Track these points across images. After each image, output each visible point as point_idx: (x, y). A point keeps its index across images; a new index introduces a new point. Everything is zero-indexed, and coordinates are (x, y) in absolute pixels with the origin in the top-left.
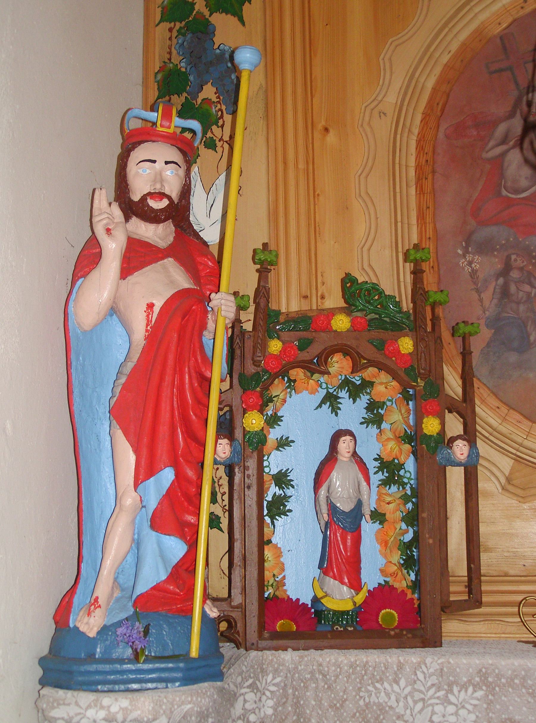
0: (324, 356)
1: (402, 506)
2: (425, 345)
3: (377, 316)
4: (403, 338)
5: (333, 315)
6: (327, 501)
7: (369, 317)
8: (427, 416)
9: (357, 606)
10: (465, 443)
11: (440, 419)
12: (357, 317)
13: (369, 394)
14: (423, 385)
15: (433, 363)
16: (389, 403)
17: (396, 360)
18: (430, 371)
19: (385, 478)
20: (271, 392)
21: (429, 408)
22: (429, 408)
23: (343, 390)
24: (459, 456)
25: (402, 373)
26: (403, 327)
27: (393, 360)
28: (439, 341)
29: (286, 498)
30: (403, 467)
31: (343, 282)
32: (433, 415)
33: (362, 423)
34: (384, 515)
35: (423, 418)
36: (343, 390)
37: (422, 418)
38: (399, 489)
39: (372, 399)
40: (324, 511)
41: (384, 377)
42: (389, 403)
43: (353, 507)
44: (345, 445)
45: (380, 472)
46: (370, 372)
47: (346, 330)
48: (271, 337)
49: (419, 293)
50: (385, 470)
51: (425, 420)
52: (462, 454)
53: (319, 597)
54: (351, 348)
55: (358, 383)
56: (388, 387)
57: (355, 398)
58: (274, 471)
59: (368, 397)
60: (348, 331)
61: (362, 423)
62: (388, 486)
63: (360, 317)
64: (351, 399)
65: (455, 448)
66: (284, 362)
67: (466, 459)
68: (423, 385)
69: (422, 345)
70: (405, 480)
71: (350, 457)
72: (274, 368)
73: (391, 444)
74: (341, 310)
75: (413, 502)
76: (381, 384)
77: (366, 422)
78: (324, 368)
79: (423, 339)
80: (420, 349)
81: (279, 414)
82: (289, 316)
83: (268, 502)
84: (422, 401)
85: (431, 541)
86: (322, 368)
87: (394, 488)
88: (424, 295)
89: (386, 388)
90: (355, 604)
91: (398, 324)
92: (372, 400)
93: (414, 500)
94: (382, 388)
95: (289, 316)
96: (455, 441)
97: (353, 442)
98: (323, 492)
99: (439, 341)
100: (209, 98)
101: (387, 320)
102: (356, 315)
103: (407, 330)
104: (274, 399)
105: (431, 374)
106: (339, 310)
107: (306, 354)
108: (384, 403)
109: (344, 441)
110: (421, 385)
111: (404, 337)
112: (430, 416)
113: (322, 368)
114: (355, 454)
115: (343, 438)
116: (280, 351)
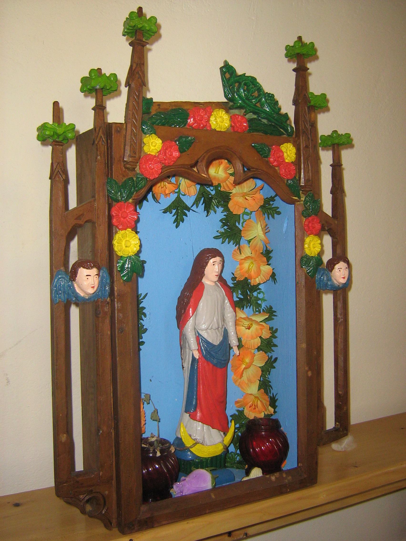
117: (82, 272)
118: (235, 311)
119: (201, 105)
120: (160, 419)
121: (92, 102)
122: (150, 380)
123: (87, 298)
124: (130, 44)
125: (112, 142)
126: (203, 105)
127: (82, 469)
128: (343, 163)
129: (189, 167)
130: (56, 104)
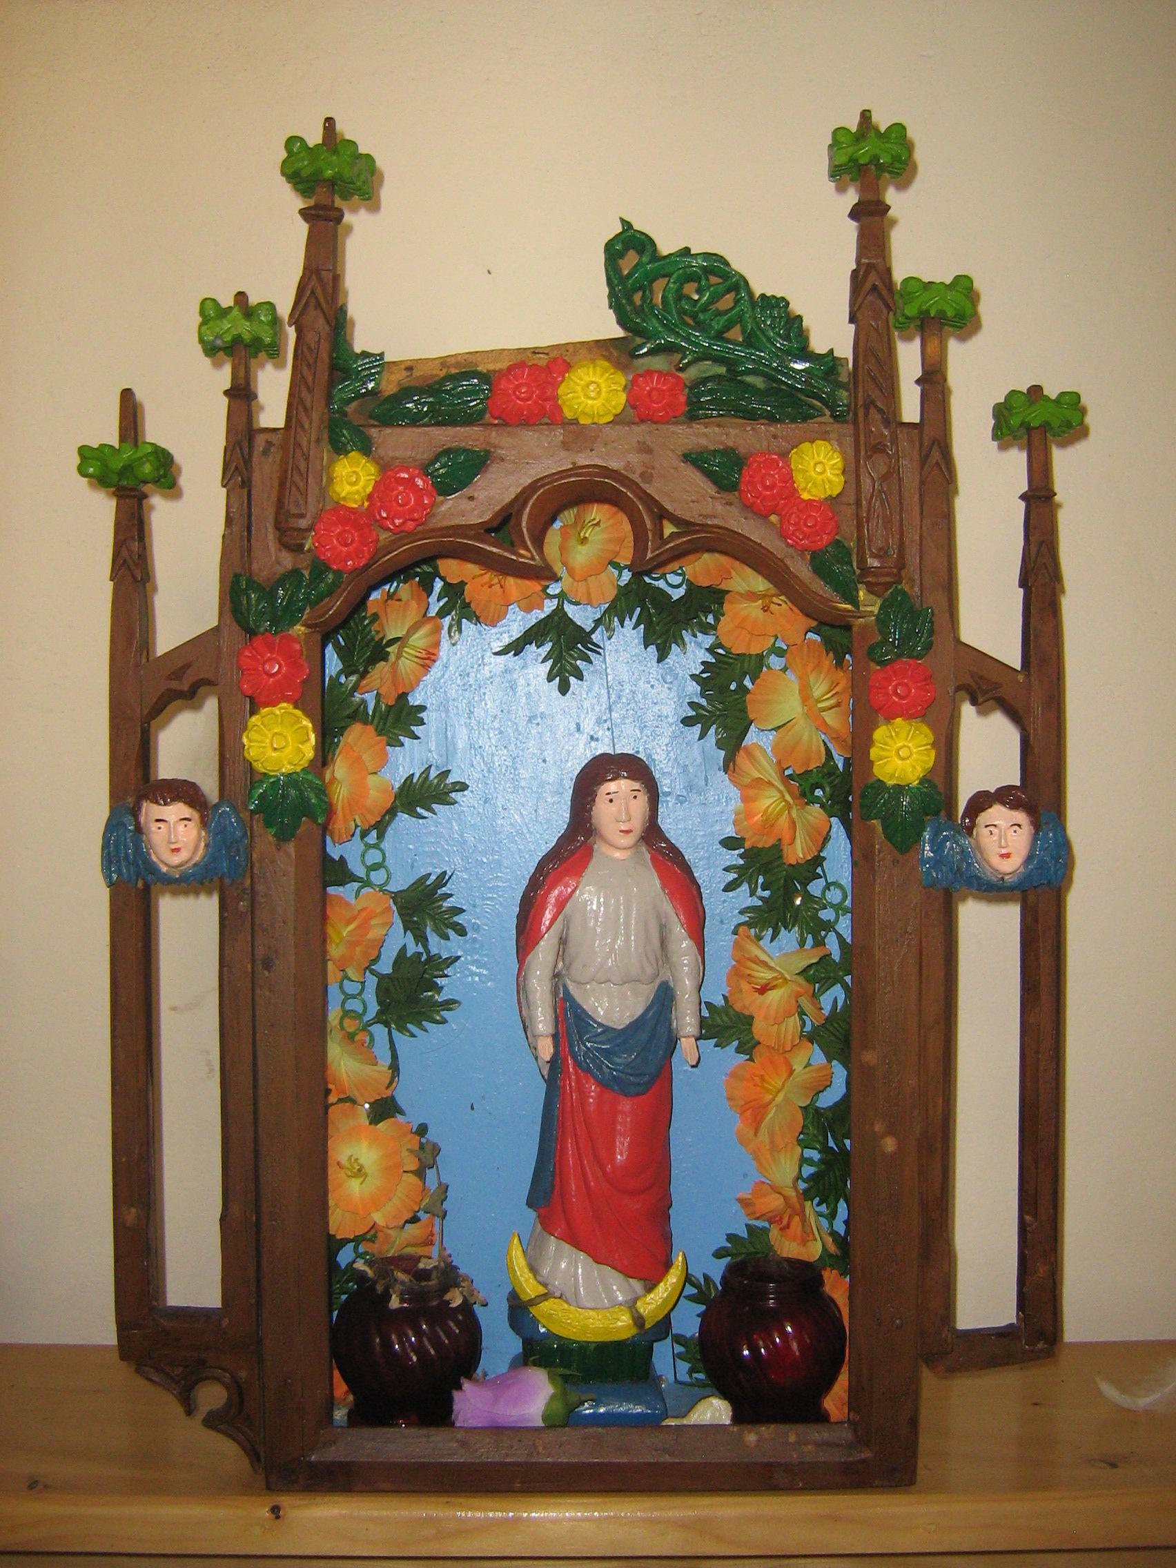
0: (528, 510)
1: (805, 1003)
2: (883, 470)
3: (722, 370)
4: (806, 446)
5: (568, 367)
6: (555, 993)
7: (692, 374)
8: (889, 718)
9: (648, 1326)
10: (1020, 817)
11: (933, 726)
12: (649, 373)
13: (706, 629)
14: (876, 612)
15: (912, 535)
16: (775, 662)
17: (781, 522)
18: (901, 565)
19: (760, 903)
20: (383, 629)
21: (895, 693)
22: (895, 693)
23: (627, 619)
24: (996, 861)
25: (801, 569)
26: (812, 407)
27: (772, 524)
28: (936, 455)
29: (441, 964)
30: (819, 870)
31: (614, 252)
32: (909, 715)
33: (687, 722)
34: (749, 1020)
35: (875, 726)
36: (627, 619)
37: (870, 727)
38: (802, 943)
39: (720, 646)
40: (540, 1026)
41: (746, 580)
42: (775, 662)
43: (639, 1011)
44: (613, 808)
45: (745, 887)
46: (703, 568)
47: (610, 418)
48: (340, 449)
49: (868, 286)
50: (761, 880)
51: (880, 734)
52: (1007, 856)
53: (524, 1298)
54: (631, 484)
55: (677, 594)
56: (773, 607)
57: (665, 642)
58: (400, 883)
59: (708, 641)
60: (618, 420)
61: (687, 722)
62: (770, 931)
63: (660, 373)
64: (652, 648)
65: (982, 832)
66: (384, 536)
67: (1022, 870)
68: (876, 609)
69: (875, 468)
70: (827, 915)
71: (636, 845)
72: (348, 556)
73: (770, 801)
74: (603, 348)
75: (845, 986)
76: (752, 596)
77: (696, 719)
78: (528, 555)
79: (878, 449)
80: (866, 483)
81: (415, 699)
82: (416, 373)
83: (382, 978)
84: (872, 664)
85: (890, 1144)
86: (522, 552)
87: (788, 938)
88: (884, 292)
89: (765, 609)
90: (639, 1320)
91: (792, 396)
92: (720, 651)
93: (848, 979)
94: (753, 610)
95: (416, 373)
96: (983, 810)
97: (643, 799)
98: (544, 952)
99: (936, 455)
100: (1051, 392)
101: (758, 382)
102: (646, 368)
103: (827, 418)
104: (388, 649)
105: (903, 573)
106: (590, 350)
107: (466, 505)
108: (761, 659)
109: (610, 797)
110: (869, 609)
111: (812, 441)
112: (899, 720)
113: (522, 552)
114: (652, 834)
115: (612, 786)
116: (370, 497)
117: (998, 815)
118: (405, 933)
119: (542, 356)
120: (446, 1213)
121: (224, 377)
122: (472, 1105)
123: (177, 876)
124: (304, 213)
125: (546, 476)
126: (547, 354)
127: (211, 1298)
128: (1056, 489)
129: (482, 531)
130: (127, 395)
